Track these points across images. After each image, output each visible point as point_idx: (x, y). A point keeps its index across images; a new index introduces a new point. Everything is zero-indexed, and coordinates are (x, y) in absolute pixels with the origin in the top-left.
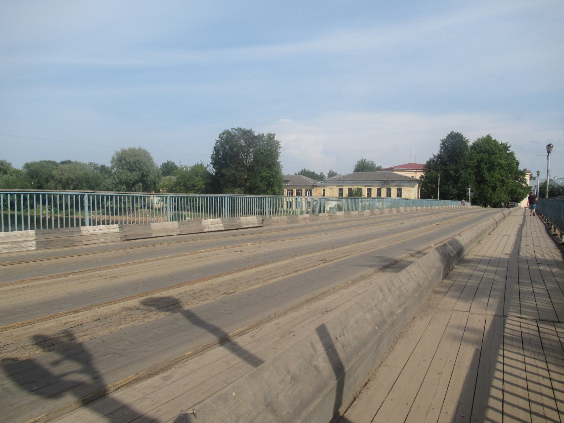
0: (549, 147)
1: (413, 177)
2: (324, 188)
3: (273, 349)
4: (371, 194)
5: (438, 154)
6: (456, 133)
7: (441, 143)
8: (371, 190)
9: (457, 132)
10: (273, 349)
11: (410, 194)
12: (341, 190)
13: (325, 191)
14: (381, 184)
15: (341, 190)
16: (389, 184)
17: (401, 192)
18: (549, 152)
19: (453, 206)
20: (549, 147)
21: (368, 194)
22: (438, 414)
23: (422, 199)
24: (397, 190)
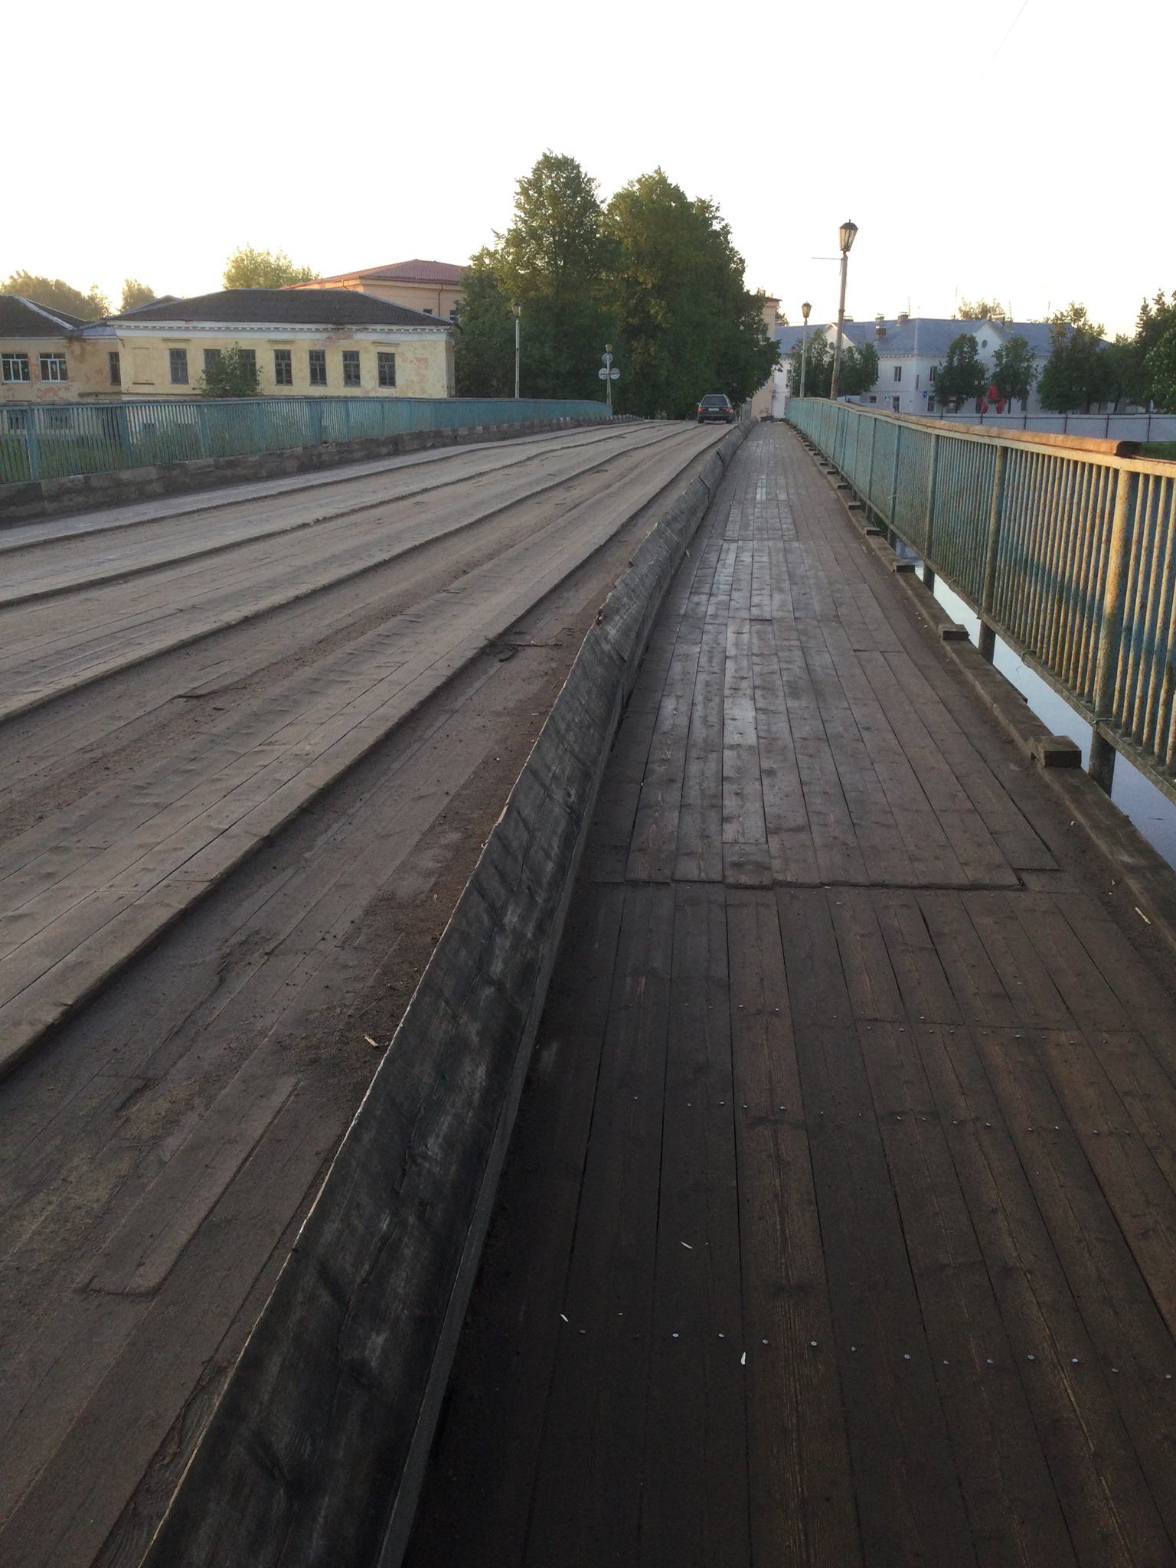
0: (850, 228)
1: (429, 311)
2: (386, 392)
3: (153, 384)
4: (289, 372)
5: (509, 230)
6: (560, 157)
7: (519, 190)
8: (289, 359)
9: (563, 156)
10: (153, 384)
11: (424, 376)
12: (387, 377)
13: (118, 360)
14: (325, 335)
15: (387, 377)
16: (352, 337)
17: (392, 368)
18: (846, 248)
19: (565, 419)
20: (850, 228)
21: (279, 373)
22: (658, 1175)
23: (526, 399)
24: (277, 358)
